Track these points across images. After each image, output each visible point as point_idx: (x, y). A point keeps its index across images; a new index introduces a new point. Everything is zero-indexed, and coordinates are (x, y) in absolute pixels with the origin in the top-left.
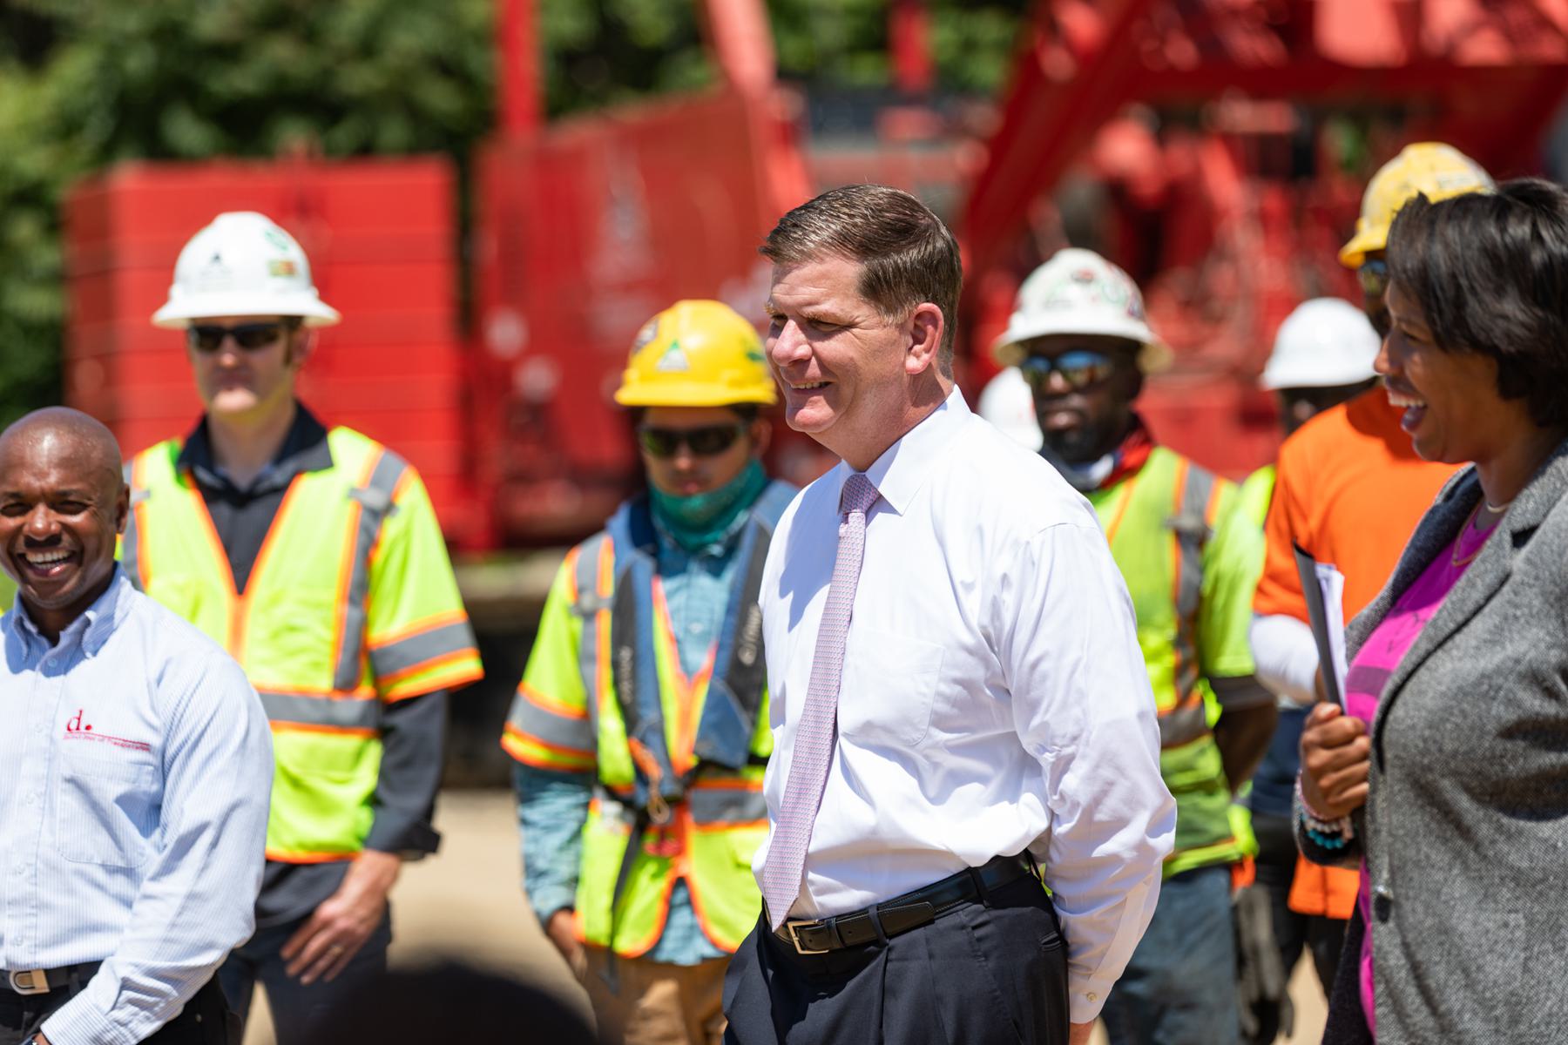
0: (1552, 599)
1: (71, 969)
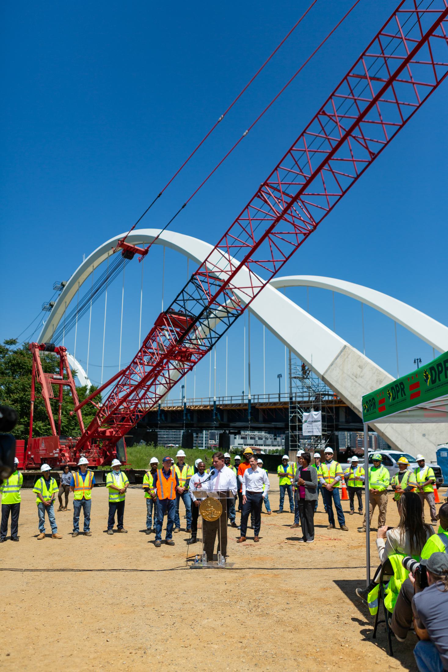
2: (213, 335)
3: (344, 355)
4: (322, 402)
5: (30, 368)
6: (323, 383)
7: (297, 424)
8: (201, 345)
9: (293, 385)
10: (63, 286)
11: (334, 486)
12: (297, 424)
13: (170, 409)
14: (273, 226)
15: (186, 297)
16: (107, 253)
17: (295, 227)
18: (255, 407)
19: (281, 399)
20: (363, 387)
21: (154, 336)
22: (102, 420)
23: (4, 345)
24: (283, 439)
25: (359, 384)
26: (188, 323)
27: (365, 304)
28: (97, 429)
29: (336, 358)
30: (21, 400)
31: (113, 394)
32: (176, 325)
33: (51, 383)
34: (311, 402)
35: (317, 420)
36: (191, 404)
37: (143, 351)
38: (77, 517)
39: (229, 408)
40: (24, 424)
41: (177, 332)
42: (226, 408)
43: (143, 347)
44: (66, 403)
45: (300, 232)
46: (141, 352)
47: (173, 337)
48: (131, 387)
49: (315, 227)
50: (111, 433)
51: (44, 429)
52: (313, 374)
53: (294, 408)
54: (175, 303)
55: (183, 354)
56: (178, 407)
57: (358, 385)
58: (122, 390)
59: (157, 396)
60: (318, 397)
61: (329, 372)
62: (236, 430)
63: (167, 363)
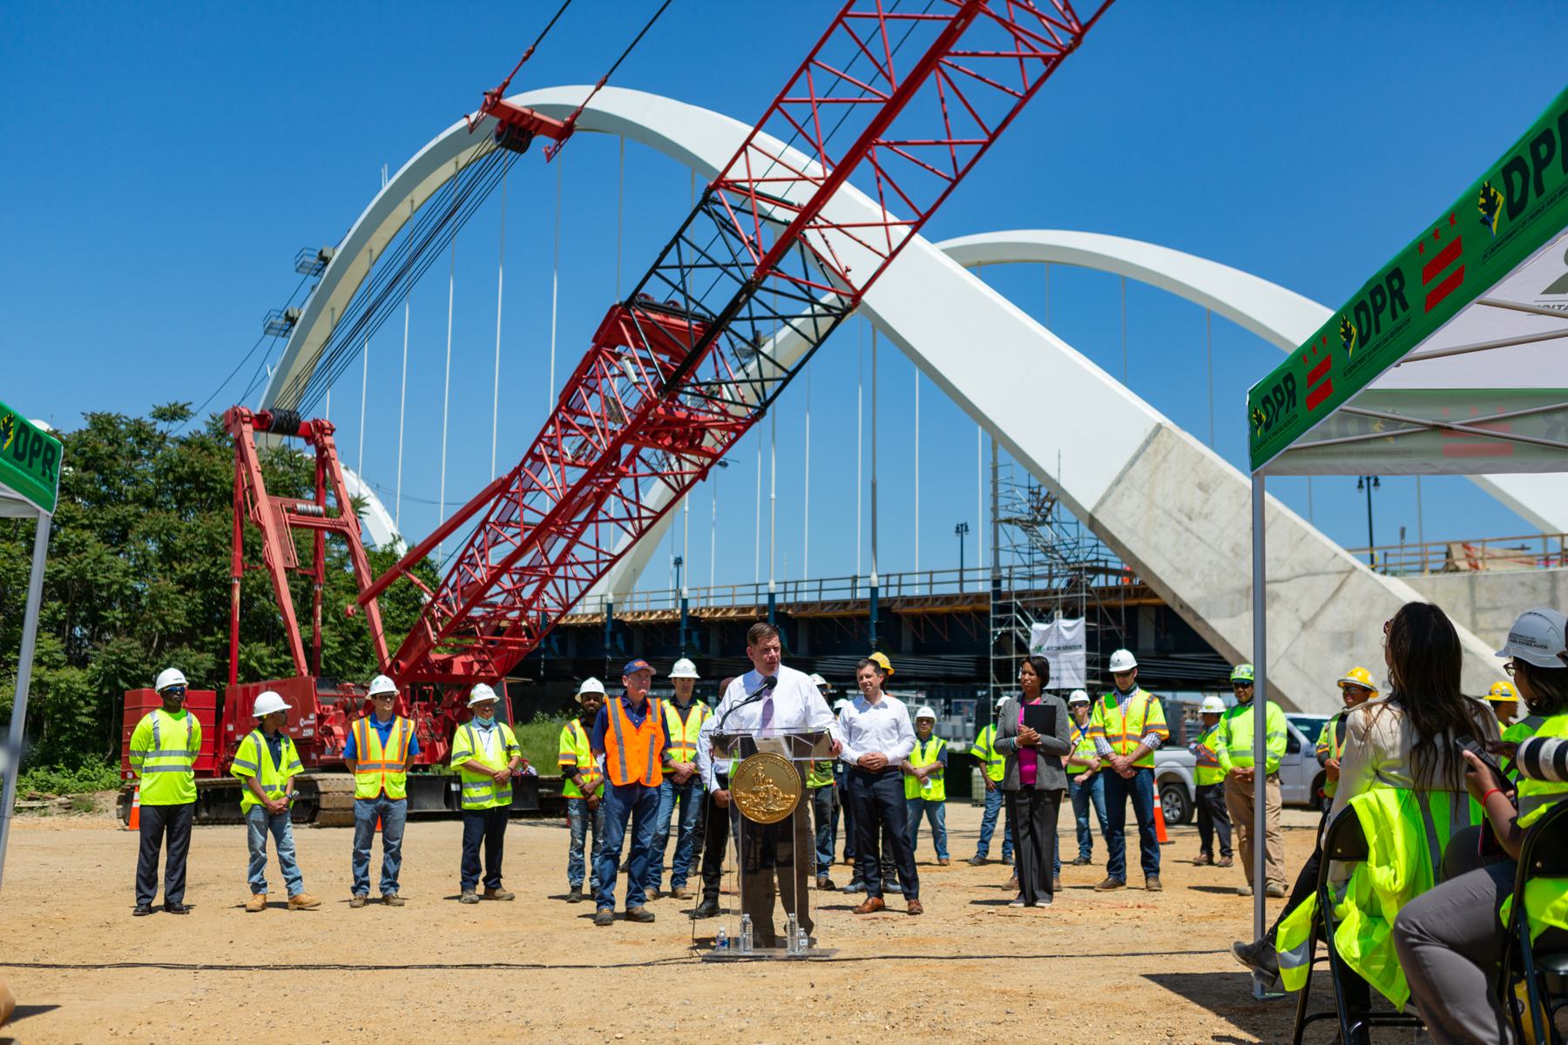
3: (1156, 452)
4: (1087, 592)
5: (228, 488)
6: (1094, 536)
7: (1014, 656)
8: (734, 402)
9: (1004, 542)
10: (325, 260)
11: (1139, 764)
12: (1014, 656)
13: (642, 618)
14: (950, 36)
15: (689, 256)
16: (454, 159)
17: (1017, 38)
18: (889, 609)
19: (965, 584)
20: (1209, 546)
21: (591, 377)
22: (441, 629)
23: (151, 421)
24: (970, 721)
25: (1199, 538)
26: (693, 338)
27: (1219, 317)
28: (425, 654)
29: (1132, 463)
30: (206, 581)
31: (470, 552)
32: (658, 346)
33: (292, 526)
34: (1056, 593)
35: (1071, 644)
36: (703, 603)
37: (562, 422)
38: (364, 852)
39: (809, 613)
40: (214, 651)
41: (662, 365)
42: (803, 614)
43: (558, 409)
44: (335, 589)
45: (1031, 53)
46: (554, 425)
47: (649, 379)
48: (526, 530)
49: (1078, 39)
50: (467, 666)
51: (271, 665)
53: (1006, 609)
54: (654, 275)
55: (677, 429)
56: (664, 613)
57: (1195, 539)
58: (502, 538)
59: (602, 557)
60: (1080, 572)
61: (1110, 501)
63: (634, 454)
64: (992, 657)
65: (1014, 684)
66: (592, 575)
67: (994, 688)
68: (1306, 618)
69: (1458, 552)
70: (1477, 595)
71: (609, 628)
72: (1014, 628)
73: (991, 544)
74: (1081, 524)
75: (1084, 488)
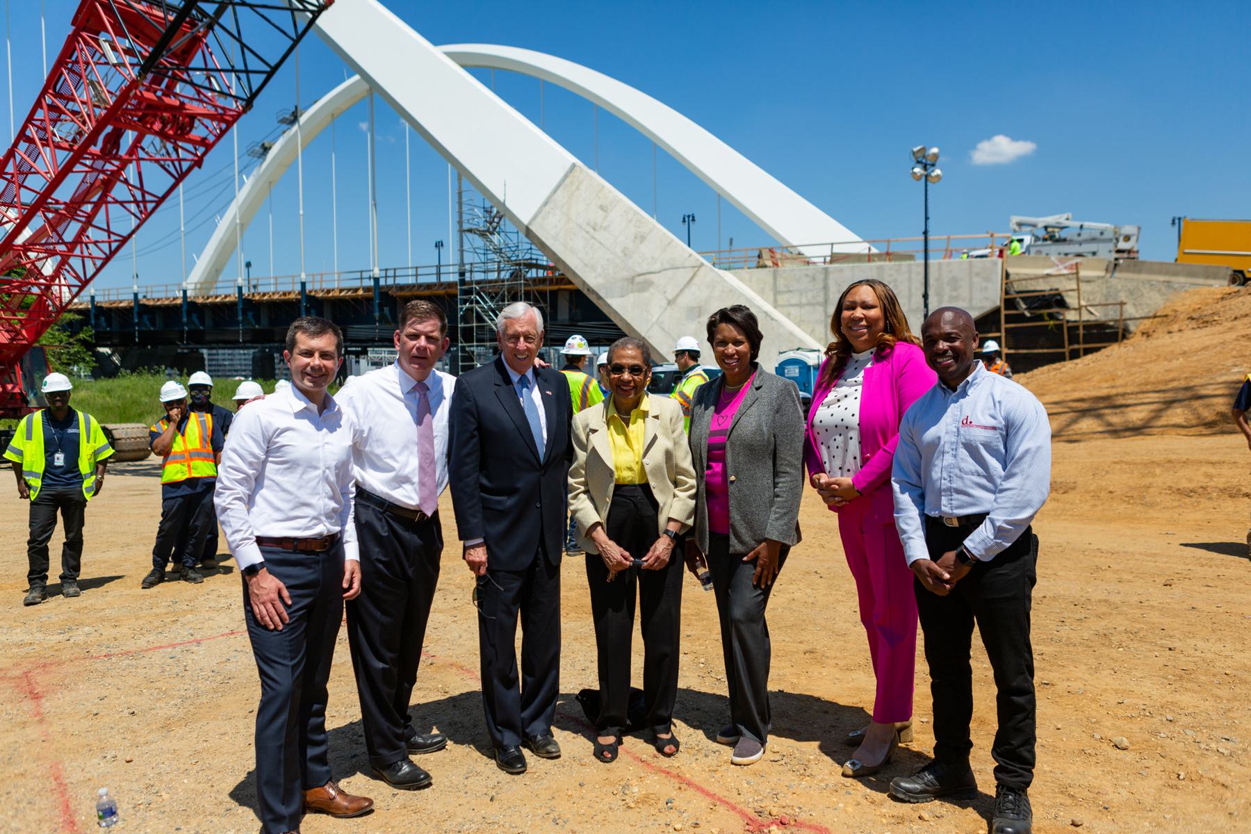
0: (186, 152)
1: (968, 517)
2: (254, 64)
6: (528, 241)
7: (474, 324)
9: (466, 246)
12: (474, 324)
13: (210, 300)
19: (442, 276)
20: (608, 249)
25: (600, 243)
29: (555, 191)
34: (503, 281)
52: (508, 222)
53: (469, 292)
55: (165, 114)
56: (226, 297)
57: (597, 244)
61: (539, 219)
62: (358, 347)
64: (460, 364)
65: (475, 344)
66: (105, 254)
67: (464, 329)
68: (670, 298)
69: (766, 255)
70: (778, 283)
71: (185, 308)
72: (474, 305)
73: (458, 247)
74: (520, 233)
75: (523, 208)
